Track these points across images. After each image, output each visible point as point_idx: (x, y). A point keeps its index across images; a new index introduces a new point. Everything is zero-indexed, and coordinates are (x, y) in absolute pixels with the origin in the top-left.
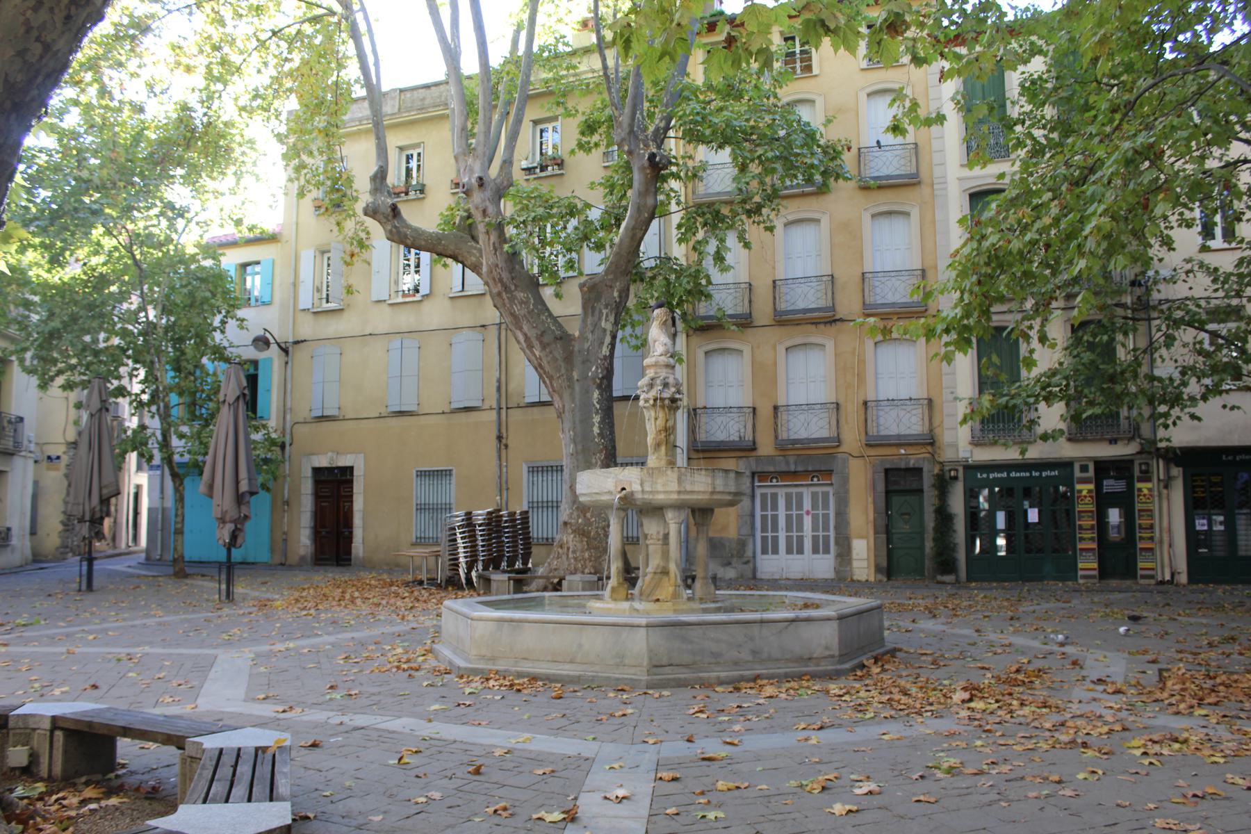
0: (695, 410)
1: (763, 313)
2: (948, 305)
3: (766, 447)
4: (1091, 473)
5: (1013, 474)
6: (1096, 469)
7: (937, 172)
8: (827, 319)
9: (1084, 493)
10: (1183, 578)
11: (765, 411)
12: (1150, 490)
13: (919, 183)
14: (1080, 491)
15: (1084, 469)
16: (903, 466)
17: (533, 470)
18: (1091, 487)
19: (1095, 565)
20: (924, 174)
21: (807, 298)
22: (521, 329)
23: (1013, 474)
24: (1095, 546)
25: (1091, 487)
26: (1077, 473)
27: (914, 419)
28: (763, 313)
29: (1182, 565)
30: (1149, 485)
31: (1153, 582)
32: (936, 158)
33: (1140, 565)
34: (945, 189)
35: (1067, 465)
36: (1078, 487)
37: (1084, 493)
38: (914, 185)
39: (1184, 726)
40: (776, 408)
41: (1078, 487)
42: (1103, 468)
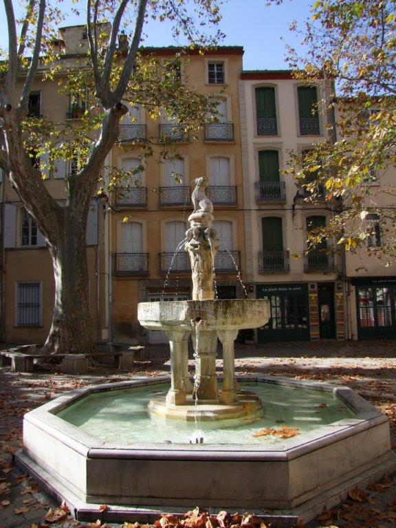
0: (116, 254)
1: (153, 201)
2: (121, 202)
3: (154, 275)
4: (316, 288)
5: (280, 289)
6: (318, 287)
7: (243, 139)
8: (140, 208)
9: (313, 298)
10: (356, 338)
11: (153, 255)
12: (342, 296)
13: (235, 144)
14: (311, 297)
15: (313, 286)
16: (226, 285)
17: (22, 285)
18: (316, 295)
19: (318, 333)
20: (237, 138)
21: (133, 198)
22: (31, 203)
23: (280, 289)
24: (317, 323)
25: (316, 295)
26: (310, 288)
27: (123, 264)
28: (153, 201)
29: (355, 332)
30: (341, 294)
31: (344, 340)
32: (243, 133)
33: (338, 332)
34: (247, 148)
35: (304, 285)
36: (310, 295)
37: (313, 298)
38: (232, 144)
39: (173, 411)
40: (159, 254)
41: (310, 295)
42: (321, 285)
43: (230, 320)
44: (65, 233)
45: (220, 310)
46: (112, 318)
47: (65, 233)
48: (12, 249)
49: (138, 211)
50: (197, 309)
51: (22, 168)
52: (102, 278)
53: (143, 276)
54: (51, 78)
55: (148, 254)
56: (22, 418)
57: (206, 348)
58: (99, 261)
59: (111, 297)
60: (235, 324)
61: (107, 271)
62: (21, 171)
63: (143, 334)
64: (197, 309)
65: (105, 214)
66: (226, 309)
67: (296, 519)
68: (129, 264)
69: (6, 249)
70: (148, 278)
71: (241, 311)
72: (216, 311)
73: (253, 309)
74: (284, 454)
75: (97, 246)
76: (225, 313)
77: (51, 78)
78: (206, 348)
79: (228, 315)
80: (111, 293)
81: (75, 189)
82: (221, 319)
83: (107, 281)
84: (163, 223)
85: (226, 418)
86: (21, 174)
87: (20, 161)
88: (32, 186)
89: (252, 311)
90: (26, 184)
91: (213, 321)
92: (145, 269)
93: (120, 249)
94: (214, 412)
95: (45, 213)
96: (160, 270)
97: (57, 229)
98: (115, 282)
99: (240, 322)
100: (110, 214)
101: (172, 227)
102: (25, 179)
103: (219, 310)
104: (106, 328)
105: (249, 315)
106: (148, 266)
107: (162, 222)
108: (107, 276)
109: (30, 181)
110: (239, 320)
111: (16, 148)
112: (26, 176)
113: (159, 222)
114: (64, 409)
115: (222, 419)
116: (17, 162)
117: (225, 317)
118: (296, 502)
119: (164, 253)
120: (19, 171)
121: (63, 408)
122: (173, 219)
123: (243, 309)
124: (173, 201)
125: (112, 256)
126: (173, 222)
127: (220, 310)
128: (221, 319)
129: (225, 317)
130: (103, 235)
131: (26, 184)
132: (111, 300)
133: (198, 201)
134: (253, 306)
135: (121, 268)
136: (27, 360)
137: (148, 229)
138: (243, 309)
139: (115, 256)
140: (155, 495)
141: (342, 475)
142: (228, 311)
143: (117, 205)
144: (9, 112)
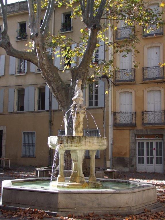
1: (139, 78)
8: (132, 82)
11: (139, 114)
27: (148, 118)
28: (139, 78)
43: (74, 145)
44: (69, 102)
45: (69, 140)
46: (113, 154)
47: (69, 102)
48: (57, 111)
49: (129, 84)
50: (60, 139)
51: (45, 67)
52: (107, 128)
53: (131, 127)
54: (71, 6)
55: (136, 113)
56: (2, 182)
57: (76, 159)
58: (105, 117)
59: (112, 140)
60: (76, 146)
61: (110, 124)
62: (46, 68)
63: (132, 165)
64: (60, 139)
65: (109, 87)
66: (72, 140)
67: (56, 214)
68: (123, 119)
69: (53, 110)
70: (135, 128)
71: (79, 141)
72: (67, 140)
73: (86, 140)
74: (57, 191)
75: (104, 107)
76: (71, 141)
77: (71, 6)
78: (76, 159)
79: (73, 142)
80: (112, 137)
81: (74, 77)
82: (69, 144)
83: (110, 129)
84: (145, 92)
85: (72, 188)
86: (45, 70)
87: (44, 63)
88: (51, 76)
89: (86, 141)
90: (48, 75)
91: (66, 145)
92: (134, 122)
93: (118, 110)
94: (68, 184)
95: (58, 91)
96: (143, 122)
97: (65, 100)
98: (115, 131)
99: (79, 146)
100: (112, 87)
101: (152, 94)
102: (48, 73)
103: (69, 140)
104: (110, 160)
105: (83, 143)
106: (135, 120)
107: (117, 92)
108: (110, 127)
109: (50, 74)
110: (78, 145)
111: (42, 56)
112: (48, 71)
113: (143, 91)
114: (22, 182)
115: (70, 188)
116: (43, 64)
117: (72, 143)
118: (61, 210)
119: (145, 111)
120: (44, 68)
121: (21, 182)
122: (152, 89)
123: (80, 140)
124: (152, 76)
125: (113, 113)
126: (124, 92)
127: (69, 140)
128: (69, 144)
129: (72, 143)
130: (108, 101)
131: (48, 75)
132: (112, 142)
133: (76, 91)
134: (86, 139)
135: (118, 122)
136: (45, 172)
137: (136, 96)
138: (80, 140)
139: (115, 114)
140: (21, 203)
141: (91, 208)
142: (73, 141)
143: (116, 81)
144: (37, 37)
